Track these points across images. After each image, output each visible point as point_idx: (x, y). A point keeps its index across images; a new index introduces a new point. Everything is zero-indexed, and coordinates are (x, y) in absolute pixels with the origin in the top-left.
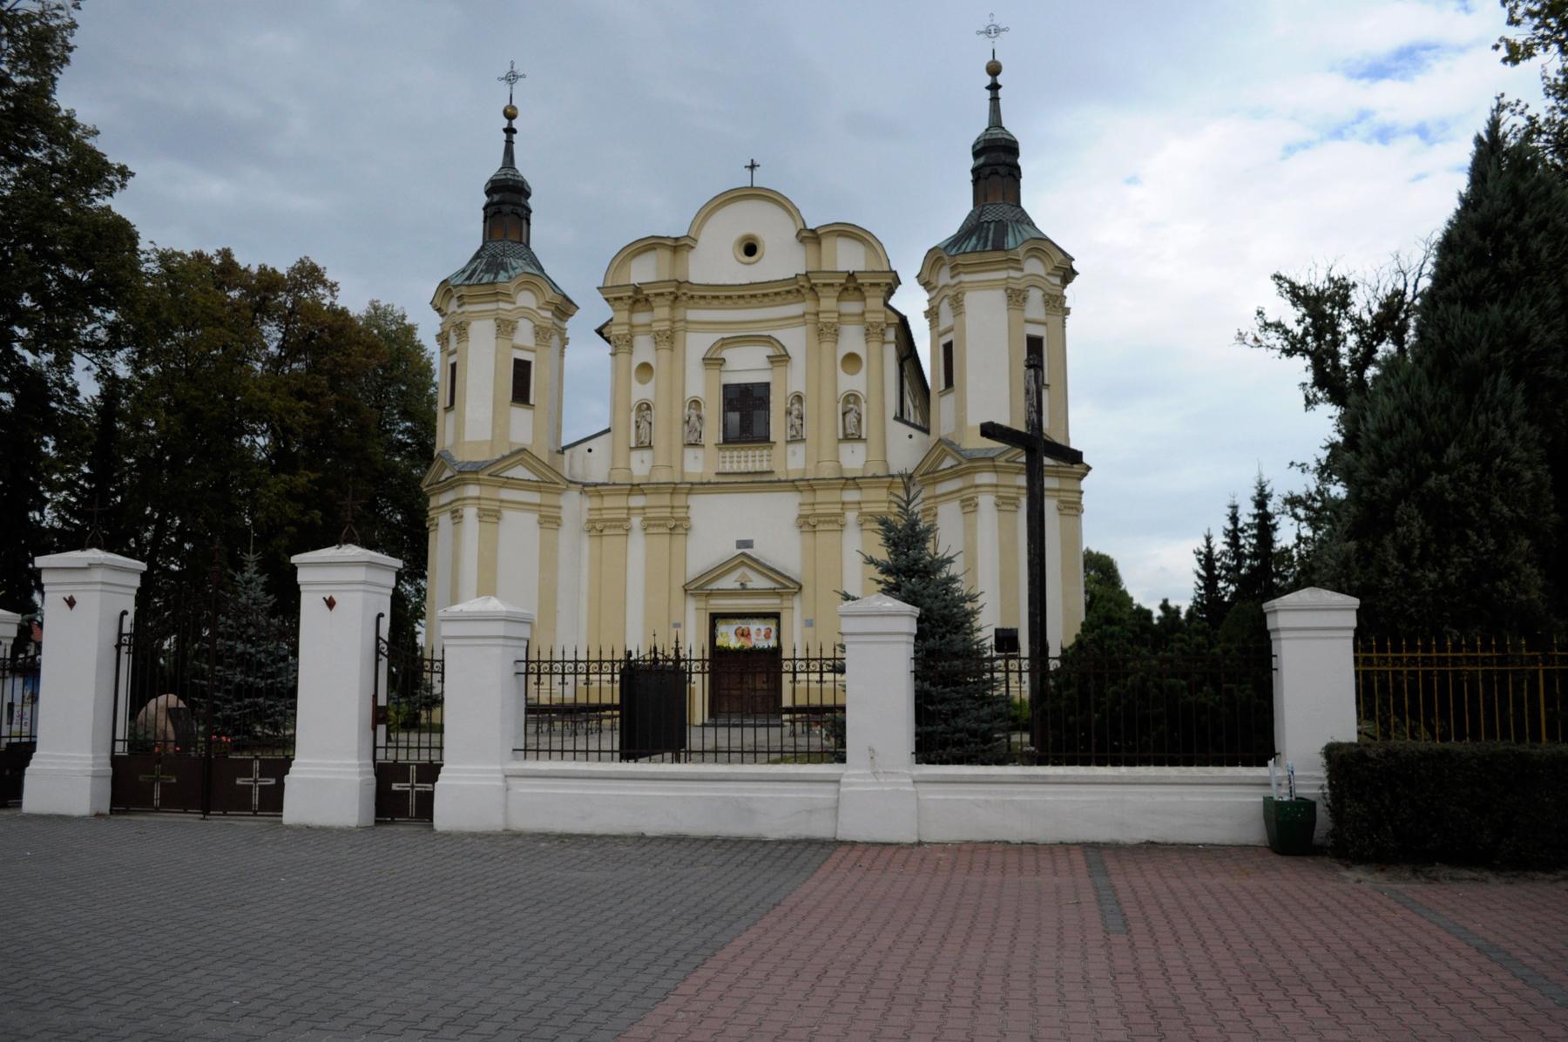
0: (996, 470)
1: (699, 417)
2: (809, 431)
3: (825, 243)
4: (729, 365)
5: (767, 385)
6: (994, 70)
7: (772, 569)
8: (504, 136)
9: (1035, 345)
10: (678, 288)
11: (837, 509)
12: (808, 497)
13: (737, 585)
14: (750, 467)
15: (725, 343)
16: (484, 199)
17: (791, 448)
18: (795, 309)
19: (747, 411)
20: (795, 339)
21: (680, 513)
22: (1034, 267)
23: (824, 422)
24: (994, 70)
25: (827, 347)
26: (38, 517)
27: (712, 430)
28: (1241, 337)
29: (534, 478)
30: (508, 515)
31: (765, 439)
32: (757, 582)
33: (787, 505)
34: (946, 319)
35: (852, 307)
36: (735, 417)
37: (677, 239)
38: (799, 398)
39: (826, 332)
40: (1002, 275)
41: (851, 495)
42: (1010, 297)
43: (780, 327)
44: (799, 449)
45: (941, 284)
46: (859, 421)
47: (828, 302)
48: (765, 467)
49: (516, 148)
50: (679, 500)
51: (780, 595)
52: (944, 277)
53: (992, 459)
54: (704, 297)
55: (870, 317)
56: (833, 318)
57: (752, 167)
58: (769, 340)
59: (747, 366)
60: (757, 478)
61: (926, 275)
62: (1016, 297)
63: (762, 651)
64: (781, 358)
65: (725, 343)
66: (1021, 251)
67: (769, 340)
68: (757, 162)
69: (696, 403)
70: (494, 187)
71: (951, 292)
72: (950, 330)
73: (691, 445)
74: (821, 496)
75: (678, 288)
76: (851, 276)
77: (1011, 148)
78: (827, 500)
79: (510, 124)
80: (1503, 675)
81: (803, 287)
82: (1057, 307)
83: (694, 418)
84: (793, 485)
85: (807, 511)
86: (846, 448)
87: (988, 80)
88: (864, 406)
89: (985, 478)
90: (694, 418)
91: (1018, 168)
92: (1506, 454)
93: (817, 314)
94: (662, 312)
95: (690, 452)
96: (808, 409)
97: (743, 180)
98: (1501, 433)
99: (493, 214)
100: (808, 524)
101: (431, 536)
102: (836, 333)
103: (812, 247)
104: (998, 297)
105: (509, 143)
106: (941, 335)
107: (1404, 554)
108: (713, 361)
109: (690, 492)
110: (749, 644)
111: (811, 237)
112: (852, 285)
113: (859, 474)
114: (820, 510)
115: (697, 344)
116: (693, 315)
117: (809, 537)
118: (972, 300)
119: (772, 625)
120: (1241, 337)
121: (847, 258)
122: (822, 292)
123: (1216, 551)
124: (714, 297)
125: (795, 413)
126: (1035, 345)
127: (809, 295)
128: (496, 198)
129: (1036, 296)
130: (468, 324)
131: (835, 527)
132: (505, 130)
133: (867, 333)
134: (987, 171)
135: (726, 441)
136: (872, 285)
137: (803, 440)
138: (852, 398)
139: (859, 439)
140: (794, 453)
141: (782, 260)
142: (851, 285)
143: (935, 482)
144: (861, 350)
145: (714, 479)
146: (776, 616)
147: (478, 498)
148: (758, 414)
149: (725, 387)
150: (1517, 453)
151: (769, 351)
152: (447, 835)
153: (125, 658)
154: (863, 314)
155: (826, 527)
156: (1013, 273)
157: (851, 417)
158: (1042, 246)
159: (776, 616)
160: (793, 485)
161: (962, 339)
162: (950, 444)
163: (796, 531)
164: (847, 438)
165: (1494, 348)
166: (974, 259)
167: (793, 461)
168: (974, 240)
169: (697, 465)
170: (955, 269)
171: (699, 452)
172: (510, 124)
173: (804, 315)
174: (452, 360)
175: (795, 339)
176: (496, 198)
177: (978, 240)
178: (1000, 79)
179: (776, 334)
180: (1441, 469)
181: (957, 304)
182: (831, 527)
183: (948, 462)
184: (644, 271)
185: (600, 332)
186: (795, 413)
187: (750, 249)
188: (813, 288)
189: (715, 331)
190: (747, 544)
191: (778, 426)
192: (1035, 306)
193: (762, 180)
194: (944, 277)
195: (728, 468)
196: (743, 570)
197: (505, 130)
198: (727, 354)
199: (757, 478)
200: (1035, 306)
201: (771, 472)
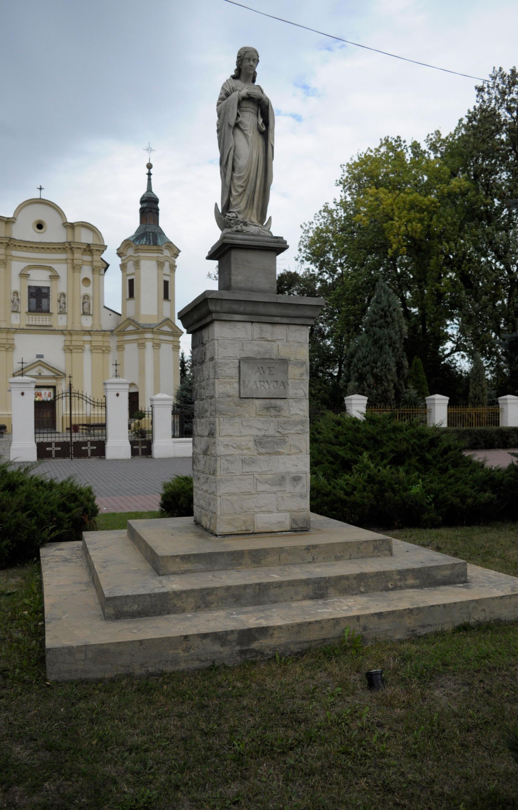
0: (153, 332)
1: (18, 300)
2: (69, 309)
3: (77, 229)
4: (31, 277)
5: (48, 288)
7: (53, 368)
8: (147, 176)
9: (166, 283)
11: (81, 343)
12: (68, 338)
13: (37, 374)
14: (41, 323)
15: (30, 267)
16: (139, 206)
17: (60, 316)
18: (63, 256)
19: (39, 298)
20: (61, 269)
21: (10, 342)
22: (167, 253)
23: (75, 306)
25: (77, 274)
27: (24, 306)
28: (209, 275)
30: (163, 346)
31: (48, 312)
32: (46, 373)
33: (59, 341)
34: (131, 269)
35: (87, 258)
36: (34, 301)
37: (8, 218)
38: (63, 295)
39: (75, 268)
40: (156, 255)
41: (87, 338)
42: (158, 264)
43: (57, 263)
44: (64, 317)
45: (128, 254)
46: (89, 307)
47: (77, 255)
48: (48, 323)
49: (152, 181)
50: (10, 336)
51: (56, 378)
52: (130, 252)
53: (152, 328)
54: (20, 246)
55: (95, 264)
56: (80, 262)
57: (41, 189)
58: (50, 269)
59: (39, 278)
60: (45, 328)
61: (122, 250)
62: (160, 265)
63: (47, 402)
64: (55, 277)
65: (30, 267)
66: (164, 246)
67: (50, 269)
68: (43, 187)
69: (16, 293)
71: (134, 259)
72: (133, 274)
73: (15, 312)
74: (74, 338)
75: (9, 241)
76: (89, 245)
77: (155, 201)
78: (77, 340)
79: (149, 171)
81: (68, 247)
82: (173, 267)
83: (16, 300)
84: (62, 332)
85: (68, 343)
86: (84, 318)
87: (147, 171)
88: (91, 301)
89: (149, 336)
90: (16, 300)
91: (158, 210)
92: (389, 365)
93: (73, 260)
95: (14, 315)
96: (69, 300)
98: (389, 360)
99: (143, 212)
100: (68, 349)
101: (500, 415)
102: (80, 269)
103: (70, 230)
104: (153, 264)
105: (149, 180)
106: (128, 275)
107: (369, 386)
108: (24, 275)
109: (15, 333)
110: (41, 399)
112: (89, 249)
113: (90, 329)
114: (74, 343)
115: (17, 267)
116: (15, 253)
117: (69, 355)
118: (143, 264)
119: (51, 391)
120: (209, 275)
122: (75, 251)
123: (186, 360)
124: (25, 247)
125: (62, 301)
126: (166, 283)
127: (69, 251)
128: (145, 205)
129: (167, 264)
131: (80, 351)
133: (93, 270)
134: (147, 210)
135: (30, 311)
136: (97, 250)
137: (65, 313)
138: (86, 297)
139: (89, 314)
140: (61, 318)
141: (54, 234)
142: (87, 249)
143: (124, 335)
144: (89, 276)
145: (25, 327)
146: (54, 388)
148: (44, 301)
149: (30, 287)
150: (392, 364)
151: (49, 273)
152: (109, 460)
154: (92, 262)
155: (77, 351)
156: (160, 255)
157: (86, 305)
158: (170, 246)
159: (54, 388)
160: (62, 332)
161: (139, 279)
162: (133, 321)
163: (62, 353)
164: (84, 313)
165: (386, 340)
166: (145, 247)
167: (61, 322)
168: (145, 240)
169: (16, 321)
170: (137, 250)
171: (18, 315)
172: (149, 171)
173: (66, 259)
174: (131, 277)
175: (61, 269)
176: (145, 205)
177: (147, 239)
179: (54, 266)
180: (377, 368)
181: (137, 264)
182: (79, 351)
183: (131, 328)
186: (62, 301)
187: (40, 226)
188: (71, 249)
189: (27, 262)
190: (41, 356)
191: (54, 307)
192: (166, 269)
193: (45, 195)
194: (130, 252)
195: (31, 323)
196: (39, 367)
198: (30, 272)
199: (45, 328)
200: (166, 269)
201: (51, 326)
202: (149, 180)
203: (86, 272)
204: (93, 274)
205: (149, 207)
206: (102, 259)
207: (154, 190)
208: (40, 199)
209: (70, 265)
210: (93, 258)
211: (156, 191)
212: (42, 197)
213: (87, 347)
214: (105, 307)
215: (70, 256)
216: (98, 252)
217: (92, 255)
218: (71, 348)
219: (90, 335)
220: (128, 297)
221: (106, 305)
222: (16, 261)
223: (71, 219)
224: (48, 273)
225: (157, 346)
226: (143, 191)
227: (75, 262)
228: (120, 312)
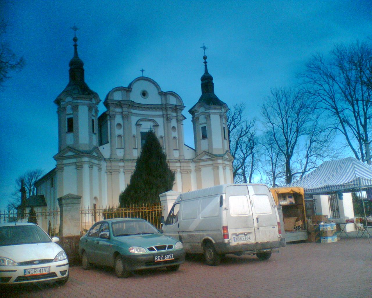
3: (168, 96)
4: (142, 126)
6: (205, 58)
8: (204, 64)
10: (131, 103)
11: (118, 168)
12: (109, 164)
16: (69, 68)
18: (160, 113)
20: (160, 121)
24: (205, 58)
26: (265, 168)
29: (74, 154)
35: (174, 114)
39: (168, 119)
40: (218, 111)
41: (121, 164)
43: (158, 117)
49: (208, 67)
55: (124, 113)
56: (114, 113)
57: (143, 71)
58: (153, 121)
59: (146, 127)
64: (156, 126)
67: (153, 121)
70: (72, 63)
73: (135, 149)
79: (75, 43)
80: (136, 212)
87: (204, 61)
94: (125, 109)
97: (140, 75)
103: (163, 97)
104: (218, 117)
105: (206, 66)
108: (138, 125)
111: (163, 94)
114: (113, 168)
115: (134, 119)
118: (81, 108)
121: (173, 101)
124: (158, 108)
130: (78, 106)
132: (204, 63)
133: (123, 118)
141: (154, 99)
147: (75, 163)
153: (315, 209)
154: (122, 112)
155: (115, 173)
172: (75, 43)
178: (207, 60)
179: (156, 119)
184: (118, 96)
185: (185, 118)
189: (139, 116)
193: (146, 75)
197: (204, 63)
198: (141, 123)
202: (206, 66)
203: (174, 123)
204: (177, 124)
205: (207, 83)
206: (182, 115)
207: (209, 72)
208: (143, 77)
209: (165, 119)
210: (123, 110)
211: (211, 72)
212: (144, 76)
213: (122, 170)
214: (185, 145)
215: (165, 113)
216: (180, 110)
217: (122, 108)
218: (111, 171)
219: (123, 161)
220: (67, 131)
221: (185, 144)
222: (134, 116)
223: (164, 90)
224: (152, 124)
225: (91, 167)
226: (71, 56)
227: (124, 113)
228: (194, 149)
